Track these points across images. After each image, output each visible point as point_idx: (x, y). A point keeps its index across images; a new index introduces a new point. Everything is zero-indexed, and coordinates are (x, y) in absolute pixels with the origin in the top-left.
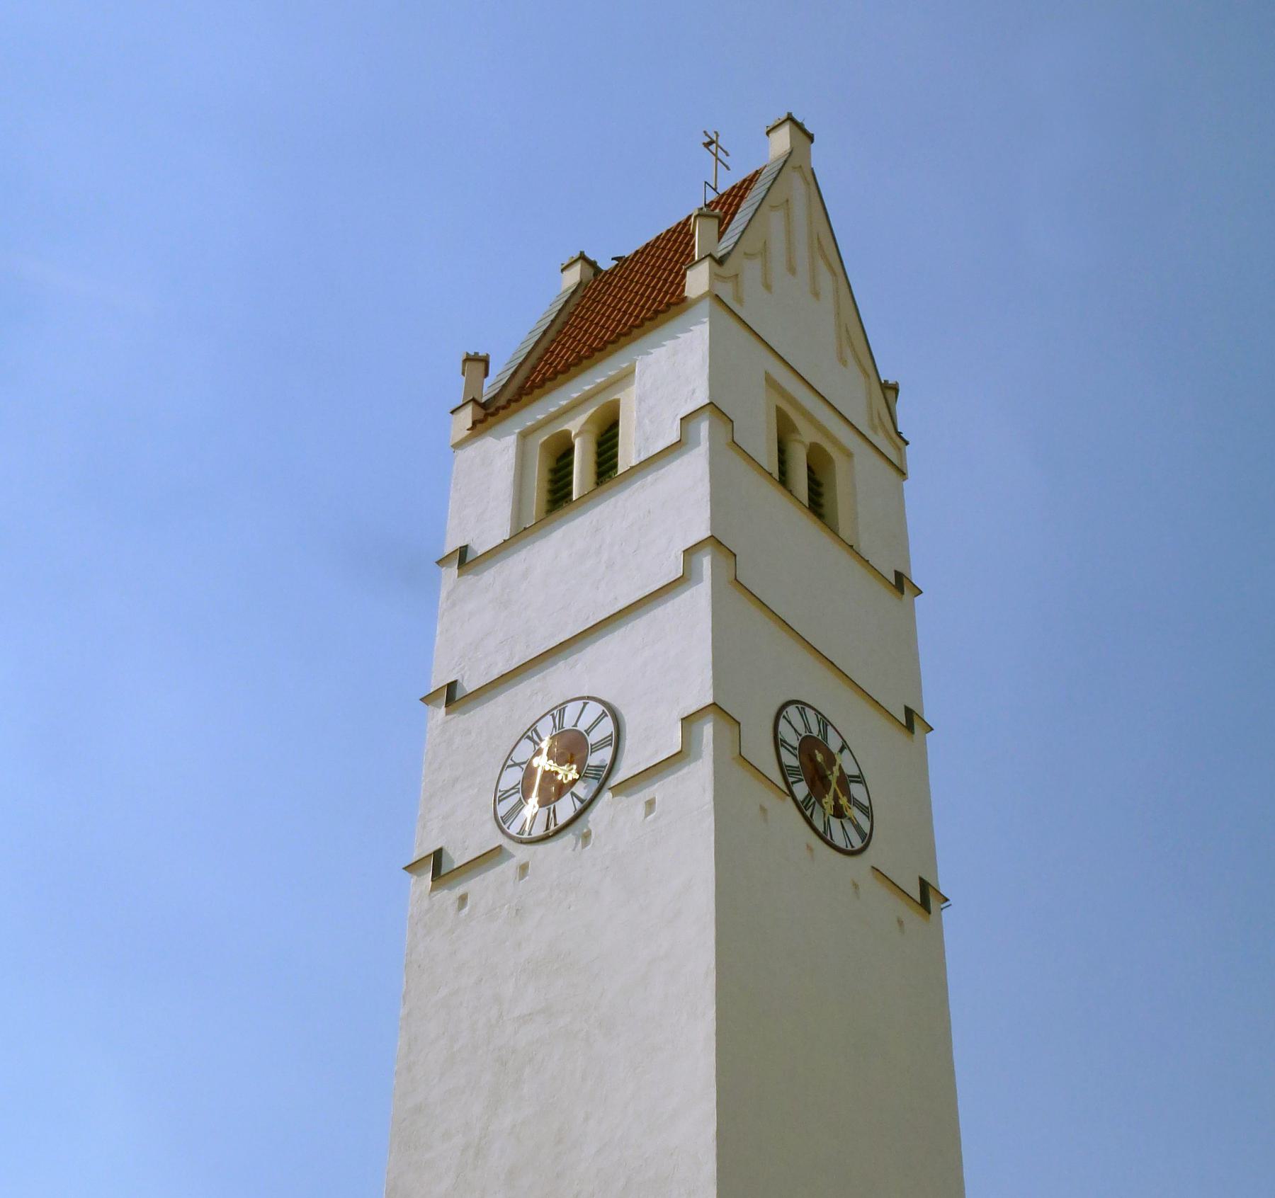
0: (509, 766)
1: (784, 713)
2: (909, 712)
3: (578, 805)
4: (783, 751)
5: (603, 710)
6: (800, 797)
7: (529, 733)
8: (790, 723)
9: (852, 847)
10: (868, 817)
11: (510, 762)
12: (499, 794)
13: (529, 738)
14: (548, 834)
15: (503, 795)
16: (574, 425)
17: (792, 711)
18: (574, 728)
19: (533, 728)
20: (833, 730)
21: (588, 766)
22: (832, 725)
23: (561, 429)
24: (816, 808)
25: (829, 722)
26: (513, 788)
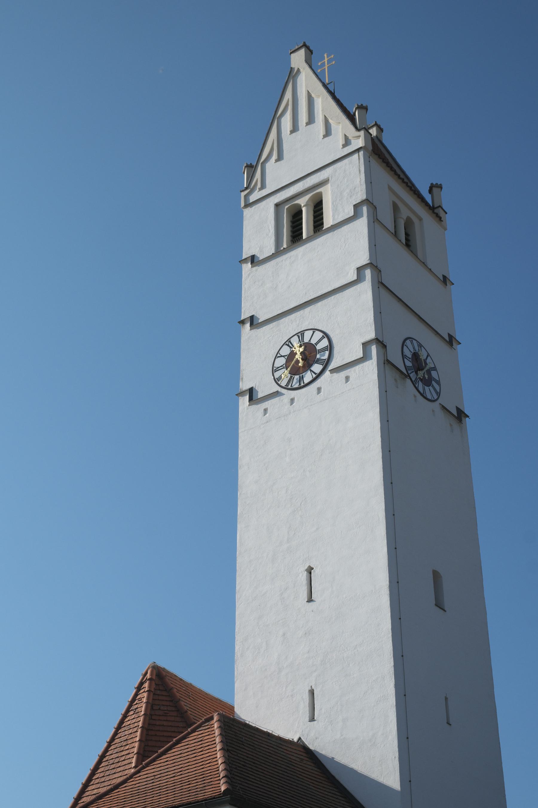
1: (405, 344)
3: (314, 376)
4: (405, 360)
5: (323, 335)
6: (413, 379)
7: (287, 343)
8: (408, 347)
9: (434, 398)
10: (438, 385)
11: (279, 355)
12: (274, 368)
13: (287, 345)
14: (301, 387)
15: (277, 369)
16: (302, 201)
17: (408, 342)
18: (309, 342)
19: (289, 340)
20: (423, 348)
21: (323, 365)
22: (423, 347)
23: (293, 203)
24: (419, 383)
25: (422, 345)
26: (281, 366)
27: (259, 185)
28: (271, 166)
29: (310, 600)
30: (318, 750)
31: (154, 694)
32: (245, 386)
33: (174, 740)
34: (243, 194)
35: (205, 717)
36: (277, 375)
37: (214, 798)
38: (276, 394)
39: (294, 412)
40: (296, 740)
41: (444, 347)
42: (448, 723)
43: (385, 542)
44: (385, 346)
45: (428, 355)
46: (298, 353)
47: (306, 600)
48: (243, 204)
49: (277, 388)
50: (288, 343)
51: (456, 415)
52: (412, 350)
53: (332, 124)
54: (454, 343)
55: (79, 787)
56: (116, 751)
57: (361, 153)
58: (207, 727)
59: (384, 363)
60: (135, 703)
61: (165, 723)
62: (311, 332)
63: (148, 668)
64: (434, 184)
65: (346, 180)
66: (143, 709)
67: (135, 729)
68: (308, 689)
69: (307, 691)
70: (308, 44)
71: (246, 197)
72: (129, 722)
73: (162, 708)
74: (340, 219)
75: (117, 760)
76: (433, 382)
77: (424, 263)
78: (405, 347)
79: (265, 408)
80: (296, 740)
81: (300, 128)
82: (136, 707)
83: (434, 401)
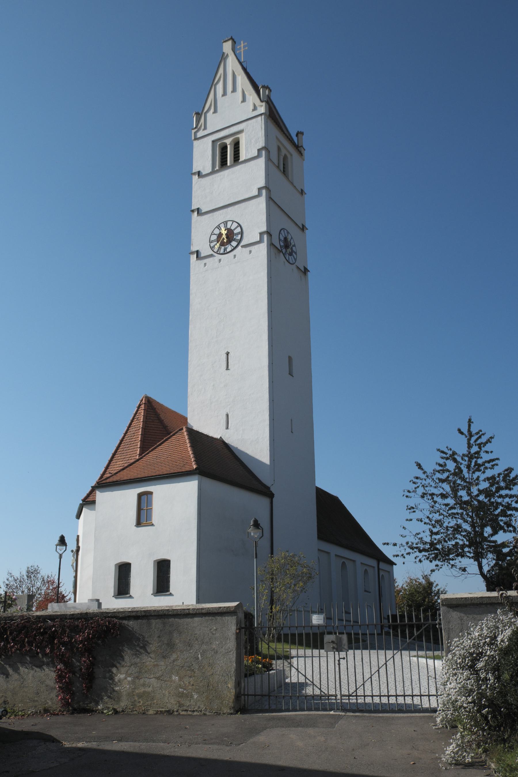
0: (213, 234)
2: (302, 190)
3: (232, 248)
4: (280, 242)
6: (284, 253)
11: (213, 233)
13: (217, 228)
16: (228, 141)
17: (282, 231)
19: (219, 226)
27: (203, 127)
28: (210, 115)
29: (227, 368)
30: (230, 443)
31: (147, 411)
32: (194, 248)
33: (164, 439)
34: (193, 131)
35: (179, 428)
36: (212, 245)
37: (190, 471)
38: (211, 256)
39: (221, 267)
40: (219, 438)
41: (299, 232)
42: (292, 432)
43: (267, 343)
44: (271, 235)
45: (292, 238)
46: (224, 234)
47: (225, 369)
48: (193, 138)
49: (211, 252)
50: (218, 227)
51: (303, 271)
52: (284, 236)
53: (246, 95)
54: (305, 230)
55: (111, 455)
56: (129, 438)
57: (263, 116)
58: (180, 434)
59: (270, 245)
60: (137, 415)
61: (153, 426)
62: (231, 222)
63: (143, 397)
64: (299, 131)
65: (253, 132)
66: (142, 418)
67: (138, 428)
68: (225, 413)
69: (225, 415)
70: (233, 37)
71: (195, 133)
72: (135, 425)
73: (151, 418)
74: (249, 157)
75: (130, 443)
76: (293, 253)
77: (292, 183)
78: (281, 235)
79: (205, 262)
80: (219, 438)
81: (228, 94)
82: (138, 417)
83: (293, 264)
